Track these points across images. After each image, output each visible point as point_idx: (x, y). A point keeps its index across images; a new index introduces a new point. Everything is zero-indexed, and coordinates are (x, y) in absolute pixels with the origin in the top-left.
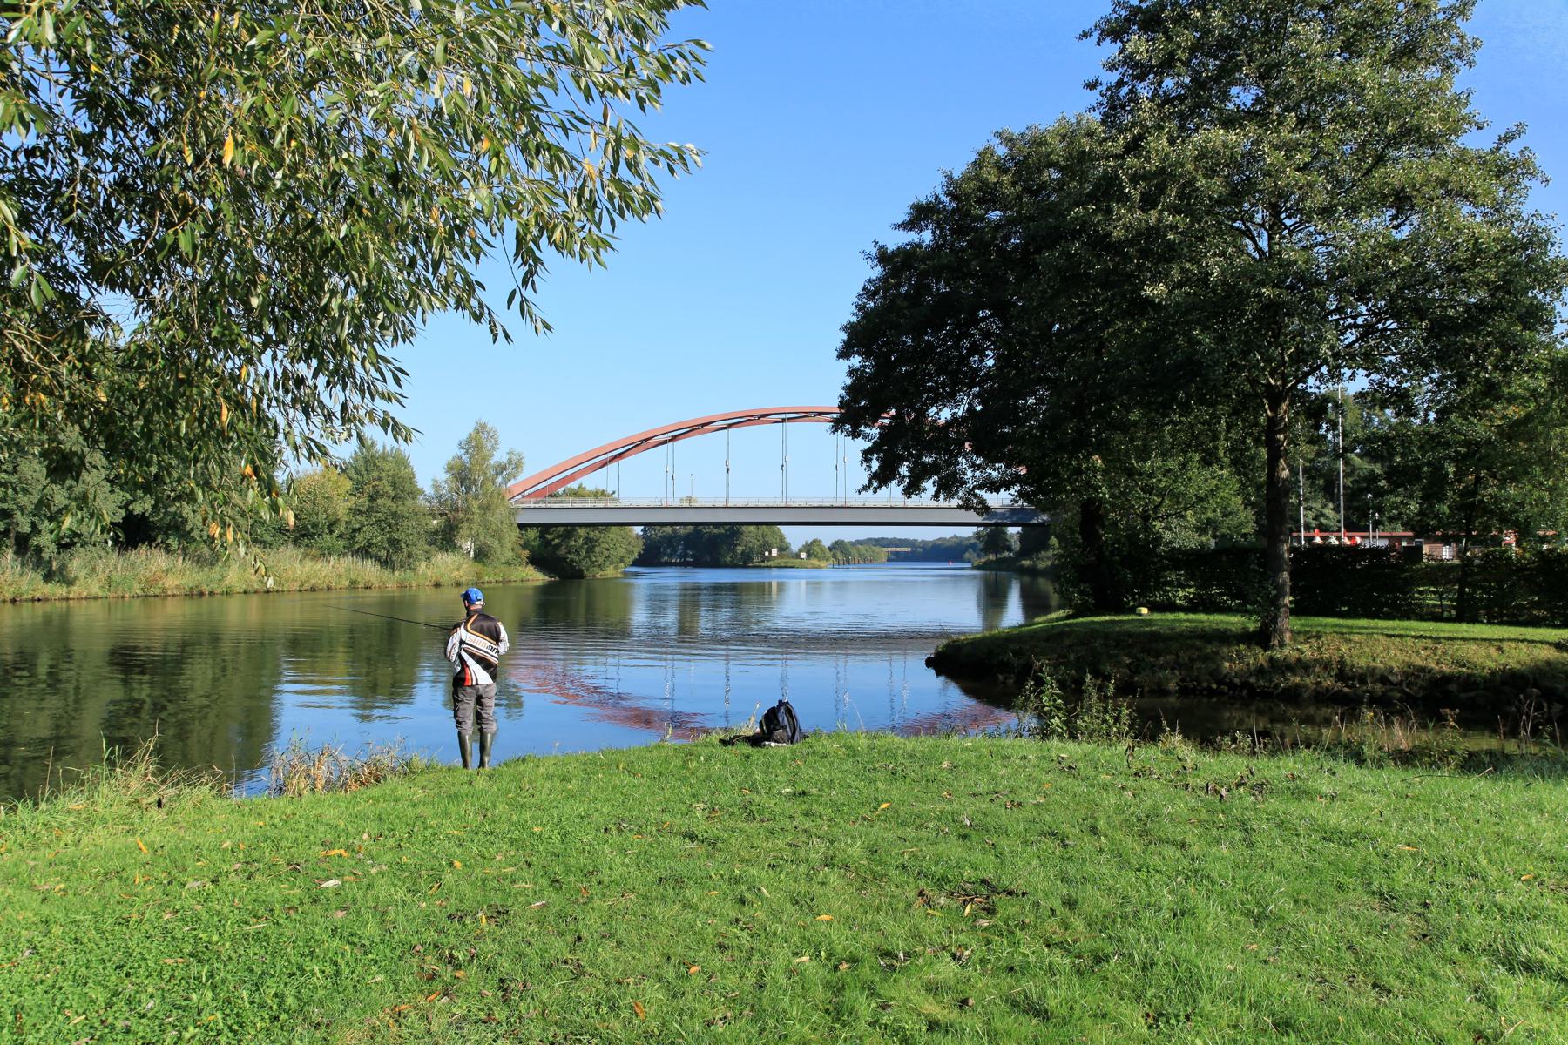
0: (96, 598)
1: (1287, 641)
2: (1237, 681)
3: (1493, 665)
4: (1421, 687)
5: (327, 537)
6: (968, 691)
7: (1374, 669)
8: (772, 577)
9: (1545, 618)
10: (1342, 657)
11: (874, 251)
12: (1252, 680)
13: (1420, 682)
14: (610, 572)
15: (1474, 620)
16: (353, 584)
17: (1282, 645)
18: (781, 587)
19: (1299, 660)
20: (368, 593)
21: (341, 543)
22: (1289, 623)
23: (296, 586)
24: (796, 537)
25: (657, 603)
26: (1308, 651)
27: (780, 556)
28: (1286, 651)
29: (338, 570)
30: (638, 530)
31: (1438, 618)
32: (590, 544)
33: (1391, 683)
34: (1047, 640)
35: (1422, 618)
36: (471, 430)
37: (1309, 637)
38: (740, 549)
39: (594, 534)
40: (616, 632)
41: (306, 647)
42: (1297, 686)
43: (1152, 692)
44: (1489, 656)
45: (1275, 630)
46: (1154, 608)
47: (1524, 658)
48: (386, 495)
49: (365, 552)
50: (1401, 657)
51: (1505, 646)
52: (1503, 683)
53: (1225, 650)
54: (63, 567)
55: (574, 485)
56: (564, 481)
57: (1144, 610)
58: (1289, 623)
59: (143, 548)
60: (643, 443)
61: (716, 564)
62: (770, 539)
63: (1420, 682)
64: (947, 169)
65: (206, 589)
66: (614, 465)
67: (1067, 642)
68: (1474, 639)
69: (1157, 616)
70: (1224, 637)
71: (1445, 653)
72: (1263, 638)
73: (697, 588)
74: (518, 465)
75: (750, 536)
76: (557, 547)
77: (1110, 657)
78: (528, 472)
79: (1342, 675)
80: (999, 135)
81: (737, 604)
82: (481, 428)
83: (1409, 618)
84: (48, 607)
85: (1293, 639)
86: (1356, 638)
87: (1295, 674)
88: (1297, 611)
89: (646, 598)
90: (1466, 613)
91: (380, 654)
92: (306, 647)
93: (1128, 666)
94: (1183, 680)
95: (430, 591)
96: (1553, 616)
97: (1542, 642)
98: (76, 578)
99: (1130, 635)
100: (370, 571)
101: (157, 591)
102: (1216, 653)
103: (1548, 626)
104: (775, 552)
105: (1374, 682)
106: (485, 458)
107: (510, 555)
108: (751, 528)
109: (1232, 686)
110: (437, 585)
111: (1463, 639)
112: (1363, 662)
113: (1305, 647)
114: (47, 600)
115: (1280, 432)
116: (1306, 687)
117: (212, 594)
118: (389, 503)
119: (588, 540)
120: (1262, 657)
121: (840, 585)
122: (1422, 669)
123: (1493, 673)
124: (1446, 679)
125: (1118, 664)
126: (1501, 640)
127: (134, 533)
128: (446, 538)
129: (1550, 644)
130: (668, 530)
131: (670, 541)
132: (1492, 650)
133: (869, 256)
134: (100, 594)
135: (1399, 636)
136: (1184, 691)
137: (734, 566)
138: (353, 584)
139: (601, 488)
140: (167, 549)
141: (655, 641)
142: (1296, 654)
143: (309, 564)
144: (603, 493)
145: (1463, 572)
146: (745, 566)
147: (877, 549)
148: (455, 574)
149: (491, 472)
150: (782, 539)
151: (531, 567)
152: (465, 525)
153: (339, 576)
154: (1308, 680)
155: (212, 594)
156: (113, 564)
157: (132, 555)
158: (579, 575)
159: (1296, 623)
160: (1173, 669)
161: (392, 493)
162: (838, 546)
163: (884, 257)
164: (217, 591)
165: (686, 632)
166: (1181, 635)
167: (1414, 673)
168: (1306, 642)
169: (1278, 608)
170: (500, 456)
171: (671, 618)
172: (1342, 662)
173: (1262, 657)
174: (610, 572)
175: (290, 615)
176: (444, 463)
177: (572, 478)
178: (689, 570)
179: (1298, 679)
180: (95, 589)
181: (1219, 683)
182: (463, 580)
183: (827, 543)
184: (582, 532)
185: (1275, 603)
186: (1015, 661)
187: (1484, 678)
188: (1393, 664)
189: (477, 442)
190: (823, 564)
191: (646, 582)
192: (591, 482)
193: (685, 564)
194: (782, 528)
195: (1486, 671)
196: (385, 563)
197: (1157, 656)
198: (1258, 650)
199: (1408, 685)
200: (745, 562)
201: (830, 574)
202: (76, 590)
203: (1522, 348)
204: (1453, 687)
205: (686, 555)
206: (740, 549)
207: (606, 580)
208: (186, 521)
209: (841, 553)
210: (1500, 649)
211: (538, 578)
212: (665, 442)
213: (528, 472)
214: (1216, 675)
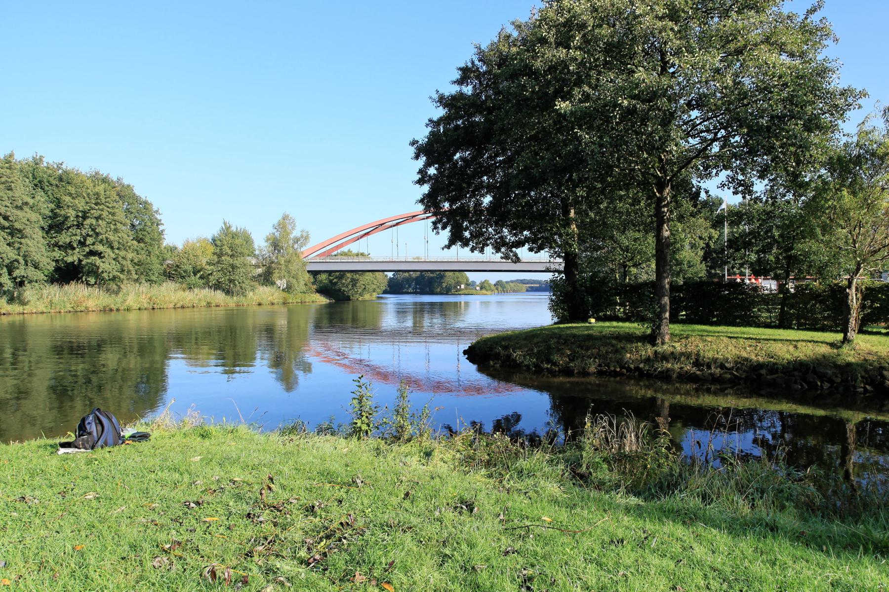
0: (42, 313)
1: (667, 340)
2: (632, 366)
3: (789, 357)
4: (744, 371)
5: (193, 278)
6: (480, 370)
7: (717, 359)
8: (462, 299)
9: (831, 327)
10: (698, 351)
11: (436, 96)
12: (641, 366)
13: (744, 367)
14: (367, 297)
15: (788, 327)
16: (209, 305)
17: (663, 343)
18: (467, 303)
19: (672, 353)
20: (218, 308)
21: (202, 281)
22: (669, 329)
23: (172, 306)
24: (472, 277)
25: (401, 312)
26: (678, 347)
27: (466, 288)
28: (665, 347)
29: (204, 295)
30: (390, 275)
31: (768, 326)
32: (354, 282)
33: (726, 368)
34: (525, 339)
35: (758, 326)
36: (280, 217)
37: (681, 337)
38: (444, 285)
39: (356, 276)
40: (373, 331)
41: (184, 340)
42: (668, 370)
43: (579, 374)
44: (788, 351)
45: (659, 334)
46: (598, 319)
47: (809, 353)
48: (226, 254)
49: (218, 286)
50: (735, 351)
51: (799, 344)
52: (795, 369)
53: (629, 346)
54: (20, 294)
55: (345, 249)
56: (337, 247)
57: (593, 320)
58: (669, 329)
59: (73, 283)
60: (380, 226)
61: (432, 293)
62: (460, 280)
63: (744, 367)
64: (476, 42)
65: (115, 308)
66: (365, 239)
67: (535, 340)
68: (781, 340)
69: (600, 324)
70: (630, 338)
71: (761, 349)
72: (651, 339)
73: (422, 304)
74: (307, 238)
75: (449, 279)
76: (336, 283)
77: (559, 350)
78: (312, 243)
79: (697, 363)
80: (513, 23)
81: (444, 315)
82: (285, 217)
83: (751, 326)
84: (10, 318)
85: (671, 339)
86: (709, 339)
87: (668, 361)
88: (674, 319)
89: (390, 313)
90: (784, 323)
91: (228, 345)
92: (184, 340)
93: (568, 356)
94: (600, 365)
95: (256, 308)
96: (837, 325)
97: (822, 343)
98: (28, 302)
99: (574, 336)
100: (219, 296)
101: (83, 309)
102: (623, 348)
103: (831, 331)
104: (463, 286)
105: (716, 368)
106: (288, 234)
107: (304, 288)
108: (451, 274)
109: (629, 369)
110: (273, 304)
111: (775, 340)
112: (710, 355)
113: (677, 345)
114: (10, 314)
115: (665, 206)
116: (673, 370)
117: (118, 310)
118: (228, 258)
119: (353, 280)
120: (648, 350)
121: (485, 304)
122: (746, 359)
123: (789, 363)
124: (761, 365)
125: (562, 355)
126: (797, 341)
127: (66, 274)
128: (267, 278)
129: (827, 343)
130: (406, 274)
131: (408, 280)
132: (791, 348)
133: (434, 100)
134: (45, 310)
135: (736, 338)
136: (600, 373)
137: (441, 294)
138: (209, 305)
139: (361, 251)
140: (88, 284)
141: (396, 335)
142: (671, 349)
143: (180, 294)
144: (362, 254)
145: (784, 298)
146: (447, 294)
147: (520, 285)
148: (270, 298)
149: (291, 242)
150: (467, 279)
151: (318, 294)
152: (277, 271)
153: (200, 300)
154: (676, 366)
155: (118, 310)
156: (54, 291)
157: (66, 287)
158: (348, 299)
159: (676, 328)
160: (595, 358)
161: (230, 253)
162: (499, 284)
163: (442, 101)
164: (122, 308)
165: (417, 332)
166: (604, 336)
167: (741, 362)
168: (679, 341)
169: (661, 320)
170: (296, 233)
171: (409, 323)
172: (698, 354)
173: (648, 350)
174: (367, 297)
175: (170, 320)
176: (264, 237)
177: (341, 246)
178: (418, 296)
179: (669, 365)
180: (41, 308)
181: (621, 368)
182: (275, 301)
183: (493, 282)
184: (349, 275)
185: (659, 316)
186: (502, 352)
187: (783, 366)
188: (729, 356)
189: (284, 225)
190: (489, 292)
191: (392, 300)
192: (354, 247)
193: (416, 293)
194: (467, 273)
195: (785, 361)
196: (228, 292)
197: (587, 349)
198: (649, 347)
199: (737, 371)
200: (447, 292)
201: (493, 298)
202: (27, 309)
203: (805, 146)
204: (763, 372)
205: (416, 288)
206: (444, 285)
207: (364, 301)
208: (98, 268)
209: (501, 287)
210: (796, 347)
211: (323, 300)
212: (391, 227)
213: (312, 243)
214: (621, 363)
